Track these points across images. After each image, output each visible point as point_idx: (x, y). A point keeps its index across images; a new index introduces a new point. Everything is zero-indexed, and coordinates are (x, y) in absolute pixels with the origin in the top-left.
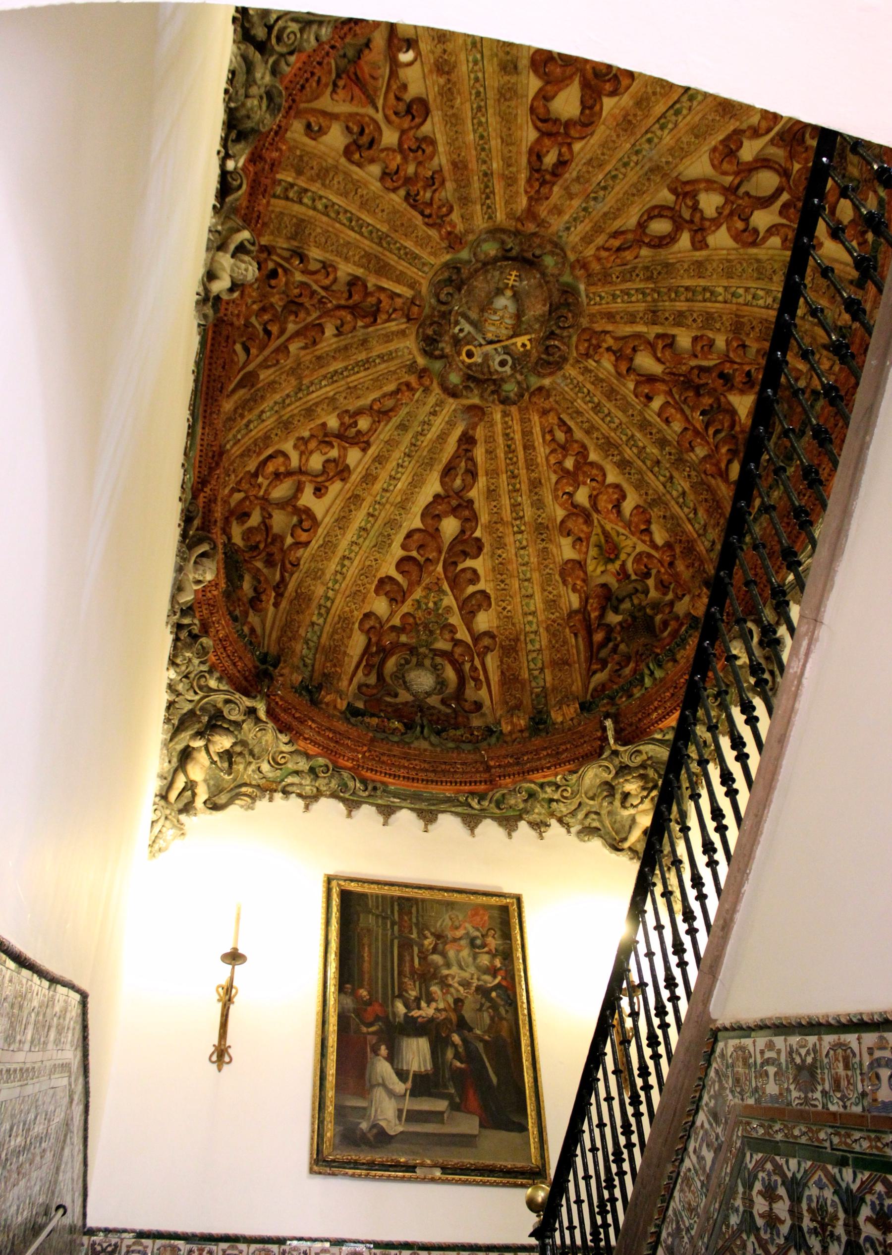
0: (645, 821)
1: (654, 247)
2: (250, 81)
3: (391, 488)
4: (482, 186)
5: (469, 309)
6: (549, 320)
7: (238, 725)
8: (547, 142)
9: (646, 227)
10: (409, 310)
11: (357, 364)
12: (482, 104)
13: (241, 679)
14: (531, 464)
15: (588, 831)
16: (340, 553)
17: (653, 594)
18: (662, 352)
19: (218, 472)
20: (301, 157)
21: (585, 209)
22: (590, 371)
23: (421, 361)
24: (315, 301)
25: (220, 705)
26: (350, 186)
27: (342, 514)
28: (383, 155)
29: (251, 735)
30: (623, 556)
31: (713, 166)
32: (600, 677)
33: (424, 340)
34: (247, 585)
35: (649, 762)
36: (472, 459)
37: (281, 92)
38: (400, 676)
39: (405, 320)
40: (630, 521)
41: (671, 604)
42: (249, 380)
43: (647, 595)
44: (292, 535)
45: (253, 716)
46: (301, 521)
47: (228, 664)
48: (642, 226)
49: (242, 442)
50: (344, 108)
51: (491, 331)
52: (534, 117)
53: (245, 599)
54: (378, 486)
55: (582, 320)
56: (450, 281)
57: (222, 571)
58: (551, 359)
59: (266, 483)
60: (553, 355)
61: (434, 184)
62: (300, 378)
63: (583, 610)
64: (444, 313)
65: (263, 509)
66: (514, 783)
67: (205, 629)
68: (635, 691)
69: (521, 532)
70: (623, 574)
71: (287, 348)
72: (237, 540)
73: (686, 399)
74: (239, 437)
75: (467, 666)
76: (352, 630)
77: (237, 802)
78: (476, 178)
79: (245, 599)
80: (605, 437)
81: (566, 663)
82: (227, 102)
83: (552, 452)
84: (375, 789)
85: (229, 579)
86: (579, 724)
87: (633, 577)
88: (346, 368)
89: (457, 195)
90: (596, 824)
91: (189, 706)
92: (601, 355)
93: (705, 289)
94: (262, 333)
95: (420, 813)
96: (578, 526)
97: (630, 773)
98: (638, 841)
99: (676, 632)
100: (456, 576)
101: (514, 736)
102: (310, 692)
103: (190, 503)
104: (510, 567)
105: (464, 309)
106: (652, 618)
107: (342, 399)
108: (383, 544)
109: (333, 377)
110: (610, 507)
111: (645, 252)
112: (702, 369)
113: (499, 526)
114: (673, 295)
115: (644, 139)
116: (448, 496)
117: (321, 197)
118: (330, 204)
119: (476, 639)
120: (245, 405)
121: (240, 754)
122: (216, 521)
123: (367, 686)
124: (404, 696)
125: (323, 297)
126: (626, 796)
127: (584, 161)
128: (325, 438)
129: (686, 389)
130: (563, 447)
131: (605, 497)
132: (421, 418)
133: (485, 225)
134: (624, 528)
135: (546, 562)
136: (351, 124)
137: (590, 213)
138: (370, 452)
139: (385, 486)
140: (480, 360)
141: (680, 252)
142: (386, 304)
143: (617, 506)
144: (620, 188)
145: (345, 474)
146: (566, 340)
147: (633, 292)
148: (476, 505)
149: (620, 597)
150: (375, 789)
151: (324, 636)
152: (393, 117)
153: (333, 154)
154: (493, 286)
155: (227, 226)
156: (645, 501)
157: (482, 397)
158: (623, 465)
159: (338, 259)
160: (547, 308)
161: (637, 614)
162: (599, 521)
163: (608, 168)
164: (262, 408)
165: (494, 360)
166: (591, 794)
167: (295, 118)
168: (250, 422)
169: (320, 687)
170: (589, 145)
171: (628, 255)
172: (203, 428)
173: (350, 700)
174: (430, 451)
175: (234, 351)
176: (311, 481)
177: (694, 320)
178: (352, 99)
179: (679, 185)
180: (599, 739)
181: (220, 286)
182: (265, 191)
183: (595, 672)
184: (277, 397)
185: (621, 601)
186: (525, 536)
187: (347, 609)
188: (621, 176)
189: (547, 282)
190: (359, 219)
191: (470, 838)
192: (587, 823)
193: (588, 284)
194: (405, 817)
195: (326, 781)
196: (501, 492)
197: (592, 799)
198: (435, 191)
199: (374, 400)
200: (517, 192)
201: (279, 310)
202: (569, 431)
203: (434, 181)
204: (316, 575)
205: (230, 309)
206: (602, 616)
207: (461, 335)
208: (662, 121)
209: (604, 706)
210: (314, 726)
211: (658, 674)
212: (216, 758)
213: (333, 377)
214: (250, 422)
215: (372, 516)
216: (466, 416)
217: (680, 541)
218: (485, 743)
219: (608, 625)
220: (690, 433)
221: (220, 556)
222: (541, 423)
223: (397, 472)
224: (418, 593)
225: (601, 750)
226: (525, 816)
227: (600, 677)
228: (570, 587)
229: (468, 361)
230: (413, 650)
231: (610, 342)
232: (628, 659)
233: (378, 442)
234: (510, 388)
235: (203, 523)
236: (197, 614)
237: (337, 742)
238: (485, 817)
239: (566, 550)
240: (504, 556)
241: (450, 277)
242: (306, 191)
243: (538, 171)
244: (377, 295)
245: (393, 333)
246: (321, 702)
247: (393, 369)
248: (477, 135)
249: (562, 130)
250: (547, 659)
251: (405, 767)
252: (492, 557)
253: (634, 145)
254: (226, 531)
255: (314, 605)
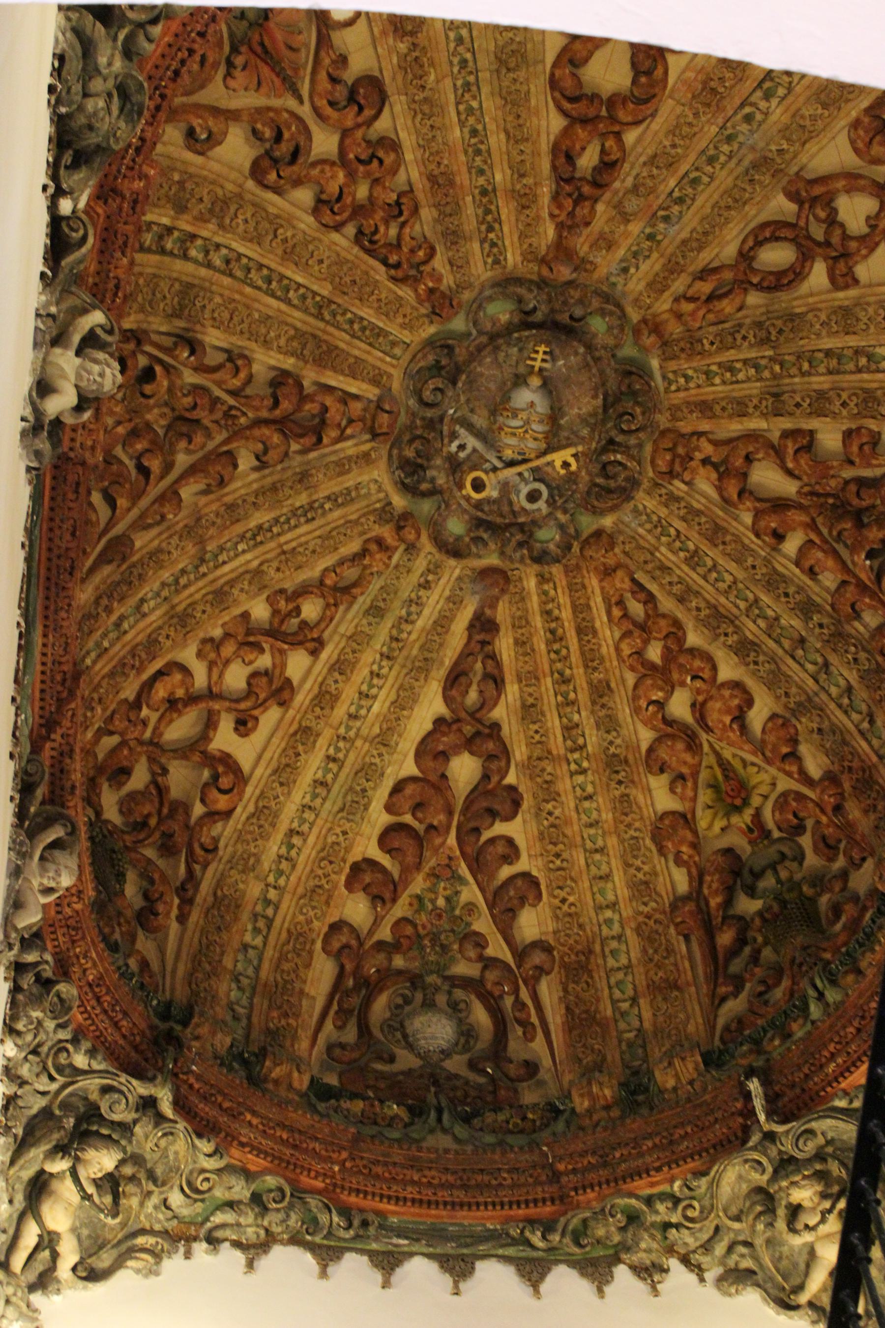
0: (829, 1254)
1: (769, 289)
2: (90, 70)
3: (363, 712)
4: (480, 211)
5: (472, 411)
6: (604, 422)
7: (125, 1128)
8: (581, 132)
9: (753, 258)
10: (374, 418)
11: (294, 512)
12: (472, 79)
13: (128, 1048)
14: (591, 660)
15: (736, 1277)
16: (283, 826)
17: (812, 860)
18: (795, 459)
19: (73, 705)
20: (181, 183)
21: (651, 237)
22: (678, 499)
23: (399, 502)
24: (218, 415)
25: (94, 1096)
26: (265, 225)
27: (284, 761)
28: (315, 172)
29: (150, 1145)
30: (756, 801)
31: (856, 151)
32: (734, 1006)
33: (401, 467)
34: (131, 889)
35: (830, 1150)
36: (492, 656)
37: (141, 85)
38: (397, 1025)
39: (368, 437)
40: (763, 741)
41: (844, 875)
42: (118, 550)
43: (801, 864)
44: (203, 801)
45: (150, 1112)
46: (216, 777)
47: (104, 1024)
48: (746, 256)
49: (112, 652)
50: (247, 100)
51: (510, 446)
52: (557, 95)
53: (129, 913)
54: (340, 711)
55: (658, 417)
56: (437, 368)
57: (88, 869)
58: (612, 484)
59: (154, 717)
60: (614, 477)
61: (401, 213)
62: (201, 542)
63: (696, 895)
64: (431, 420)
65: (151, 760)
66: (601, 1198)
67: (63, 969)
68: (795, 1026)
69: (584, 772)
70: (758, 830)
71: (176, 493)
72: (112, 814)
73: (840, 534)
74: (106, 644)
75: (509, 1001)
76: (311, 953)
77: (130, 1263)
78: (469, 199)
79: (129, 913)
80: (710, 606)
81: (675, 986)
82: (54, 106)
83: (624, 636)
84: (365, 1224)
85: (100, 880)
86: (705, 1090)
87: (776, 834)
88: (276, 521)
89: (439, 228)
90: (747, 1263)
91: (42, 1102)
92: (694, 471)
93: (858, 352)
94: (134, 472)
95: (446, 1262)
96: (676, 754)
97: (798, 1171)
98: (824, 1289)
99: (855, 922)
100: (481, 851)
101: (595, 1117)
102: (245, 1063)
103: (29, 761)
104: (568, 832)
105: (464, 411)
106: (813, 900)
107: (272, 572)
108: (354, 806)
109: (256, 536)
110: (727, 719)
111: (754, 299)
112: (861, 482)
113: (544, 763)
114: (806, 366)
115: (739, 117)
116: (458, 720)
117: (218, 246)
118: (232, 256)
119: (521, 953)
120: (111, 594)
121: (132, 1179)
122: (73, 787)
123: (342, 1046)
124: (406, 1060)
125: (231, 408)
126: (795, 1210)
127: (642, 159)
128: (248, 637)
129: (840, 518)
130: (643, 627)
131: (718, 705)
132: (405, 594)
133: (489, 274)
134: (754, 753)
135: (628, 819)
136: (259, 126)
137: (659, 242)
138: (324, 655)
139: (353, 710)
140: (495, 494)
141: (812, 295)
142: (335, 413)
143: (740, 718)
144: (705, 199)
145: (286, 695)
146: (635, 452)
147: (738, 365)
148: (505, 731)
149: (757, 868)
150: (365, 1224)
151: (266, 965)
152: (328, 111)
153: (234, 175)
154: (508, 372)
155: (64, 306)
156: (786, 706)
157: (502, 554)
158: (744, 649)
159: (253, 345)
160: (600, 401)
161: (787, 896)
162: (711, 745)
163: (684, 168)
164: (140, 595)
165: (518, 492)
166: (734, 1210)
167: (166, 122)
168: (122, 618)
169: (262, 1054)
170: (650, 134)
171: (727, 306)
172: (45, 636)
173: (315, 1072)
174: (422, 648)
175: (90, 504)
176: (229, 710)
177: (844, 404)
178: (259, 84)
179: (801, 185)
180: (741, 1114)
181: (60, 403)
182: (125, 244)
183: (723, 1000)
184: (166, 575)
185: (757, 875)
186: (590, 777)
187: (301, 918)
188: (706, 179)
189: (596, 360)
190: (282, 277)
191: (533, 1302)
192: (731, 1263)
193: (665, 358)
194: (420, 1272)
195: (281, 1216)
196: (546, 708)
197: (737, 1218)
198: (403, 225)
199: (326, 570)
200: (538, 218)
201: (161, 432)
202: (650, 599)
203: (401, 208)
204: (247, 864)
205: (79, 439)
206: (728, 902)
207: (462, 455)
208: (767, 85)
209: (743, 1056)
210: (255, 1121)
211: (832, 996)
212: (90, 1189)
213: (256, 536)
214: (122, 618)
215: (334, 760)
216: (478, 587)
217: (850, 769)
218: (546, 1134)
219: (741, 918)
220: (851, 588)
221: (84, 843)
222: (602, 589)
223: (371, 686)
224: (418, 884)
225: (746, 1133)
226: (624, 1256)
227: (734, 1006)
228: (671, 857)
229: (475, 496)
230: (415, 980)
231: (708, 449)
232: (779, 972)
233: (336, 638)
234: (548, 535)
235: (52, 792)
236: (49, 945)
237: (295, 1147)
238: (557, 1262)
239: (660, 797)
240: (557, 812)
241: (438, 362)
242: (193, 237)
243: (569, 181)
244: (319, 398)
245: (349, 459)
246: (265, 1080)
247: (354, 517)
248: (466, 130)
249: (604, 113)
250: (641, 981)
251: (413, 1183)
252: (537, 815)
253: (723, 127)
254: (92, 801)
255: (245, 916)
